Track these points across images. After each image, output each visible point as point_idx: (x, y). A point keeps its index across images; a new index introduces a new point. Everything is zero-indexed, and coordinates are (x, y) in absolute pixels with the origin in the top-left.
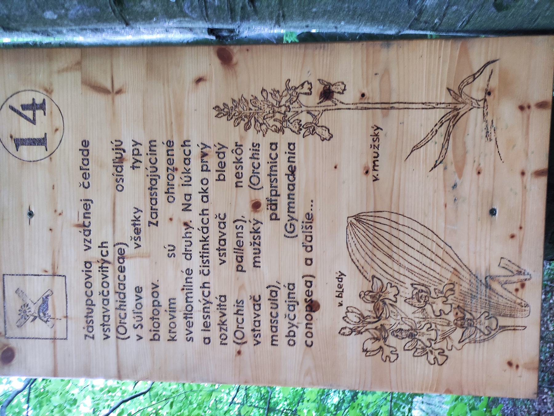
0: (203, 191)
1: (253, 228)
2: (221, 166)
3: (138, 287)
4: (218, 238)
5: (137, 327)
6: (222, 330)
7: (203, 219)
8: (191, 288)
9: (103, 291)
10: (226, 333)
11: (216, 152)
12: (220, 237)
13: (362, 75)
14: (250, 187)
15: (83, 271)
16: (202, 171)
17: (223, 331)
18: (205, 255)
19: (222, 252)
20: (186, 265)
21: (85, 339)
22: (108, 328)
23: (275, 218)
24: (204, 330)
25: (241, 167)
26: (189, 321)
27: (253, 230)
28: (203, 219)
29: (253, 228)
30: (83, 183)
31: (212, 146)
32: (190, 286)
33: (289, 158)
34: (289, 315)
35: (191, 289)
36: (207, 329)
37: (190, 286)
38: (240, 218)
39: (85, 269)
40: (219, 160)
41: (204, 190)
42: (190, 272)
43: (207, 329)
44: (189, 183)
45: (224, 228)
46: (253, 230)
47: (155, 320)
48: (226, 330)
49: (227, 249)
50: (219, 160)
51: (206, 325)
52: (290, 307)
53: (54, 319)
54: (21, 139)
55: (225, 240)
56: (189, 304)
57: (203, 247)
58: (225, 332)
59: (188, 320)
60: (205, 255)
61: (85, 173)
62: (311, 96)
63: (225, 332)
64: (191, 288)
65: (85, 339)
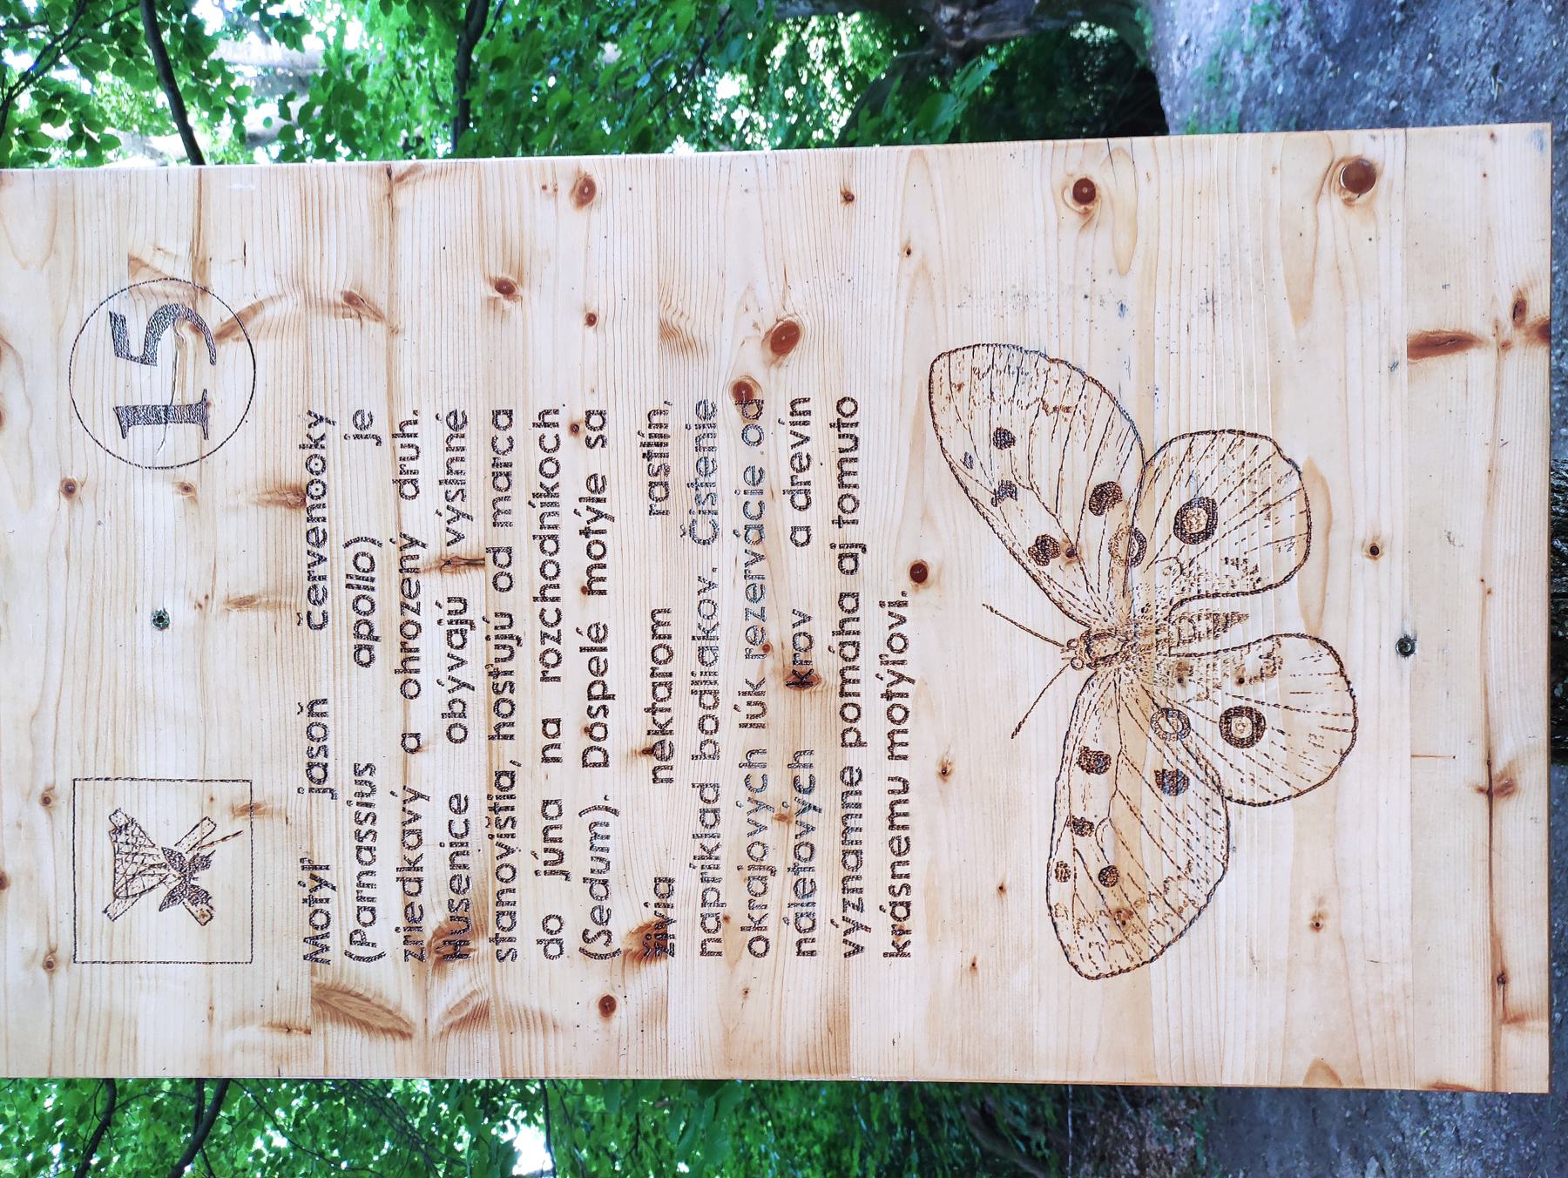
1: (309, 436)
3: (597, 625)
4: (399, 828)
5: (368, 766)
7: (543, 610)
12: (404, 824)
13: (788, 560)
17: (550, 644)
18: (503, 803)
20: (1082, 601)
23: (593, 417)
24: (745, 726)
26: (898, 838)
27: (307, 442)
28: (543, 610)
29: (309, 436)
31: (386, 542)
33: (698, 439)
36: (598, 645)
38: (602, 803)
43: (598, 645)
45: (462, 647)
46: (307, 442)
48: (544, 636)
52: (705, 697)
60: (503, 803)
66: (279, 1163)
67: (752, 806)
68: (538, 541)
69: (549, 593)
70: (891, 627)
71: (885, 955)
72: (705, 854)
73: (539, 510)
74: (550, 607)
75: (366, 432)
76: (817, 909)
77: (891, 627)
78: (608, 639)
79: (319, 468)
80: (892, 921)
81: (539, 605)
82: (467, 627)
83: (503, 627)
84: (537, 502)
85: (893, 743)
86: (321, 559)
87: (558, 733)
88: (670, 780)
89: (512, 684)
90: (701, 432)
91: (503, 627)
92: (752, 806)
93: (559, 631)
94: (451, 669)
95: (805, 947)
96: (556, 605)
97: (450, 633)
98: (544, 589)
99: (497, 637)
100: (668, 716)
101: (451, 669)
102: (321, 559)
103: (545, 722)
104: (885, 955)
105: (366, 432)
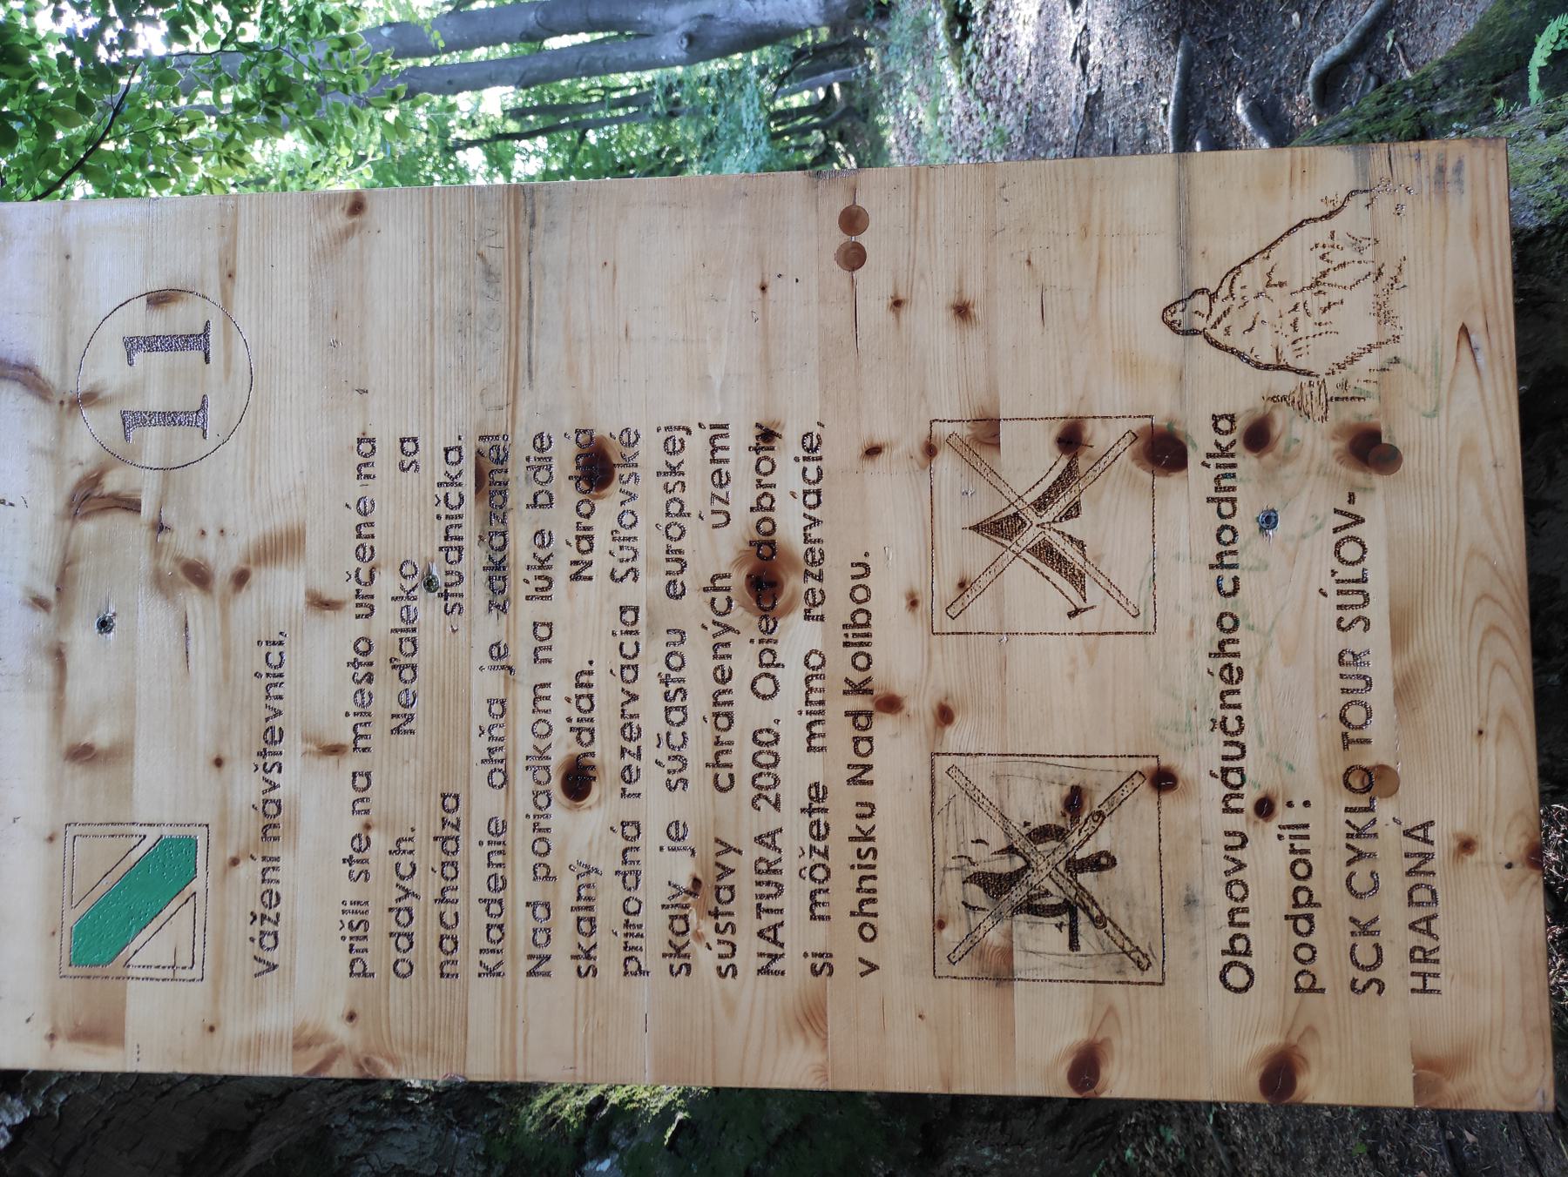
0: (860, 835)
2: (720, 677)
8: (866, 640)
9: (1225, 719)
11: (1287, 917)
30: (668, 734)
32: (1347, 593)
34: (668, 734)
35: (867, 635)
37: (1347, 593)
40: (402, 686)
41: (862, 832)
42: (633, 438)
44: (548, 593)
47: (762, 454)
51: (627, 734)
54: (131, 785)
56: (543, 716)
57: (1410, 896)
59: (815, 816)
61: (1229, 666)
64: (866, 640)
66: (1237, 3)
69: (1227, 560)
70: (622, 503)
72: (448, 480)
73: (1215, 472)
74: (1228, 575)
77: (622, 503)
79: (1238, 781)
80: (666, 541)
83: (1232, 758)
84: (1212, 462)
86: (634, 698)
88: (1228, 834)
89: (875, 851)
91: (1232, 758)
94: (718, 854)
95: (542, 655)
96: (1233, 573)
98: (1220, 555)
101: (718, 854)
102: (634, 698)
103: (403, 441)
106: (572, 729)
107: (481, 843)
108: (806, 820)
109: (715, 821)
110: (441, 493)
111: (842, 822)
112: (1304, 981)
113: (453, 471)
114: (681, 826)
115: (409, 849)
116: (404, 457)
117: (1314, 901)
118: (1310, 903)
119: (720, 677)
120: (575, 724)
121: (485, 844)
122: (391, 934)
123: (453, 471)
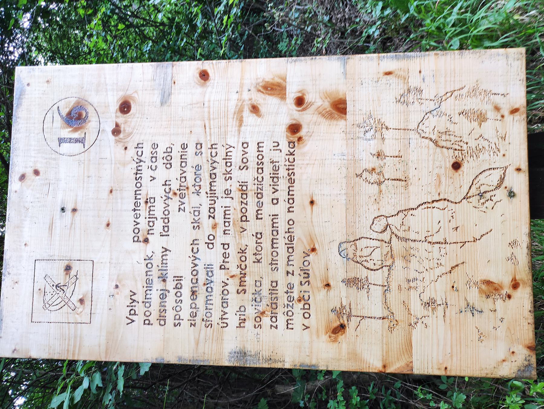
2: (275, 169)
6: (272, 327)
10: (293, 310)
14: (166, 228)
15: (270, 185)
16: (134, 241)
17: (243, 205)
19: (274, 266)
21: (209, 218)
22: (198, 226)
25: (293, 174)
39: (272, 183)
40: (224, 251)
48: (246, 204)
49: (45, 66)
50: (224, 251)
53: (426, 100)
55: (215, 174)
58: (246, 206)
62: (42, 307)
63: (246, 206)
65: (209, 218)
67: (166, 198)
68: (272, 179)
71: (151, 181)
75: (229, 196)
76: (187, 160)
78: (279, 171)
81: (164, 187)
82: (155, 219)
83: (212, 204)
85: (258, 214)
87: (168, 231)
90: (274, 217)
91: (212, 204)
92: (166, 198)
93: (247, 201)
97: (149, 222)
99: (149, 218)
100: (260, 256)
104: (151, 181)
105: (229, 196)
106: (271, 177)
107: (146, 218)
108: (286, 296)
109: (107, 349)
110: (287, 157)
111: (282, 226)
112: (244, 218)
113: (292, 150)
114: (150, 280)
115: (153, 209)
116: (177, 298)
117: (181, 318)
118: (179, 319)
119: (275, 169)
120: (272, 175)
121: (147, 218)
122: (206, 243)
123: (292, 150)
